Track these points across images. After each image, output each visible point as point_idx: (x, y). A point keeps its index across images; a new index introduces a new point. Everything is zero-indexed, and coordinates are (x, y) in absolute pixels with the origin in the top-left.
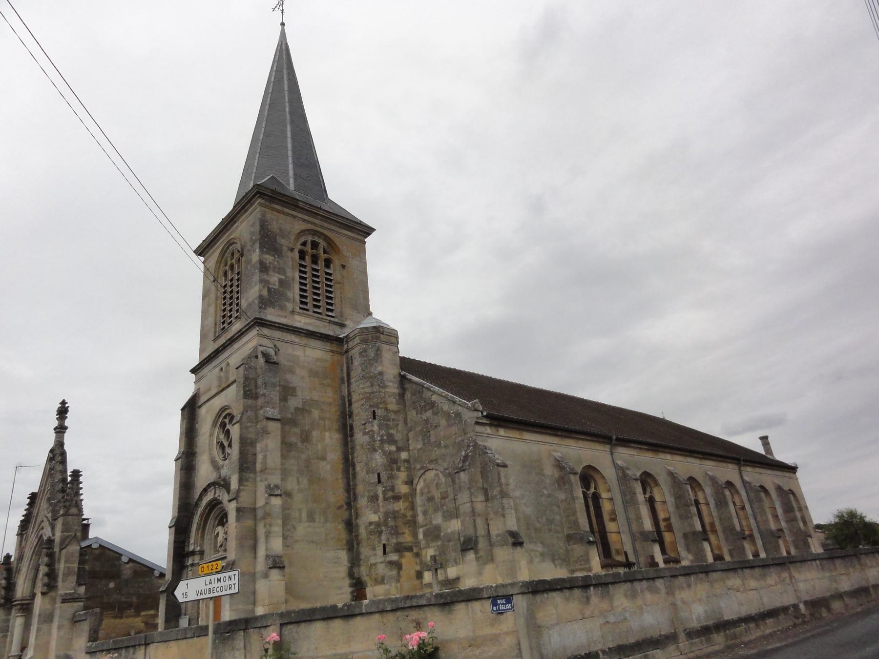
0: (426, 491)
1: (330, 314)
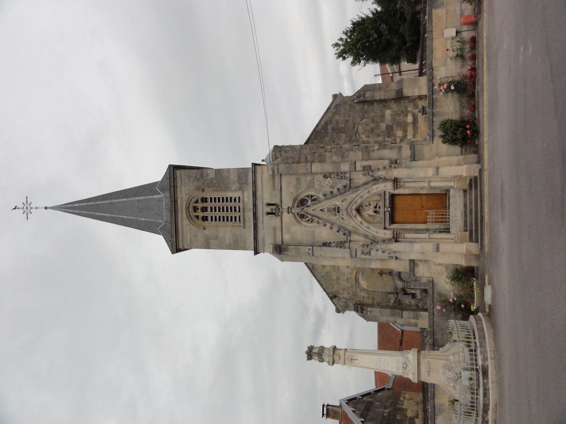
0: (367, 133)
1: (237, 209)
